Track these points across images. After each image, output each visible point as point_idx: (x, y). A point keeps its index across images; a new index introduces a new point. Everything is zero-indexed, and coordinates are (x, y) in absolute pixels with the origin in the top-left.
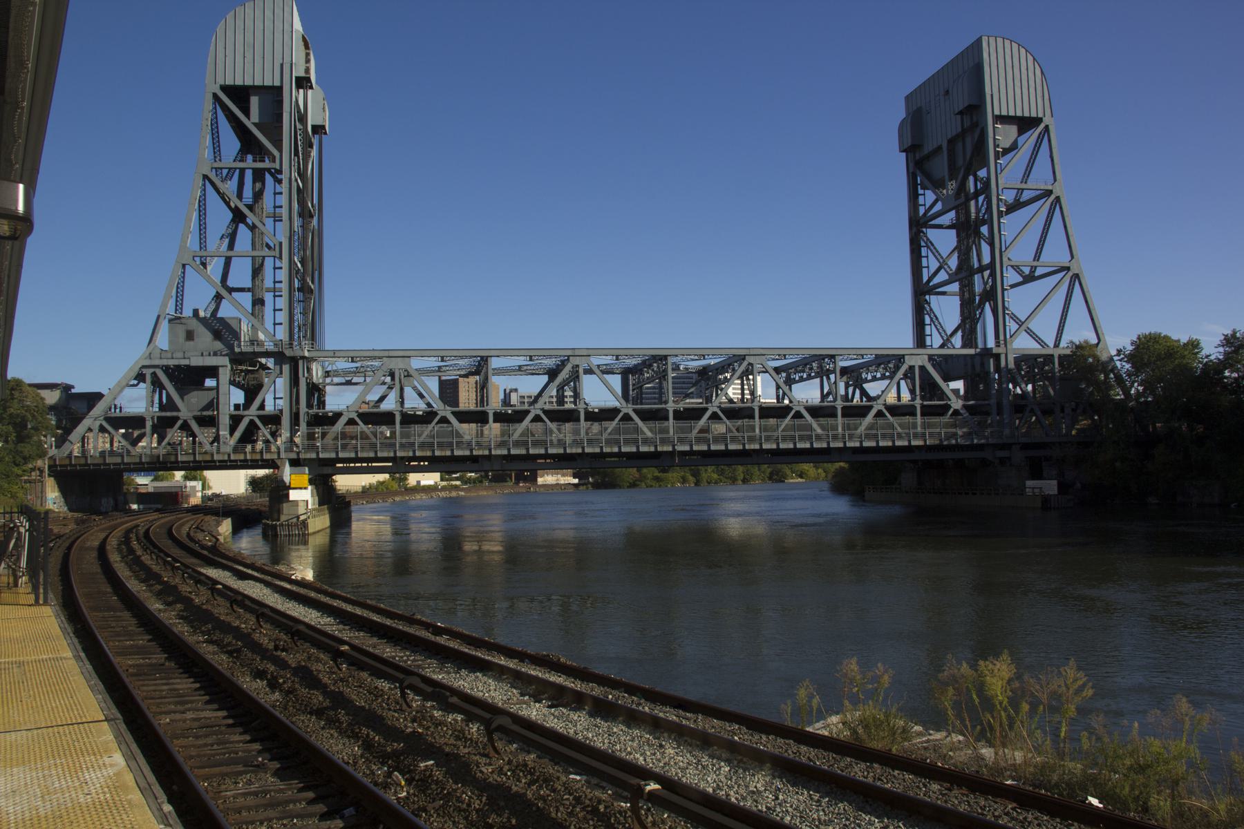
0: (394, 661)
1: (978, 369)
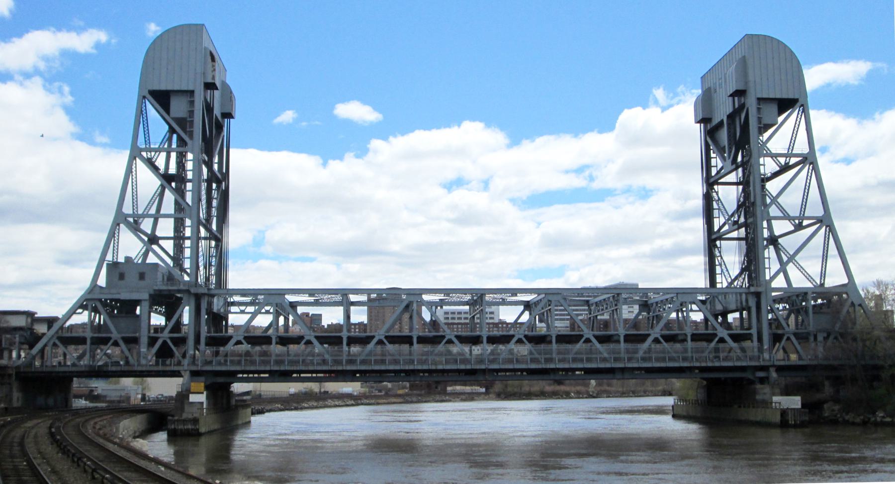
0: (66, 369)
1: (744, 304)
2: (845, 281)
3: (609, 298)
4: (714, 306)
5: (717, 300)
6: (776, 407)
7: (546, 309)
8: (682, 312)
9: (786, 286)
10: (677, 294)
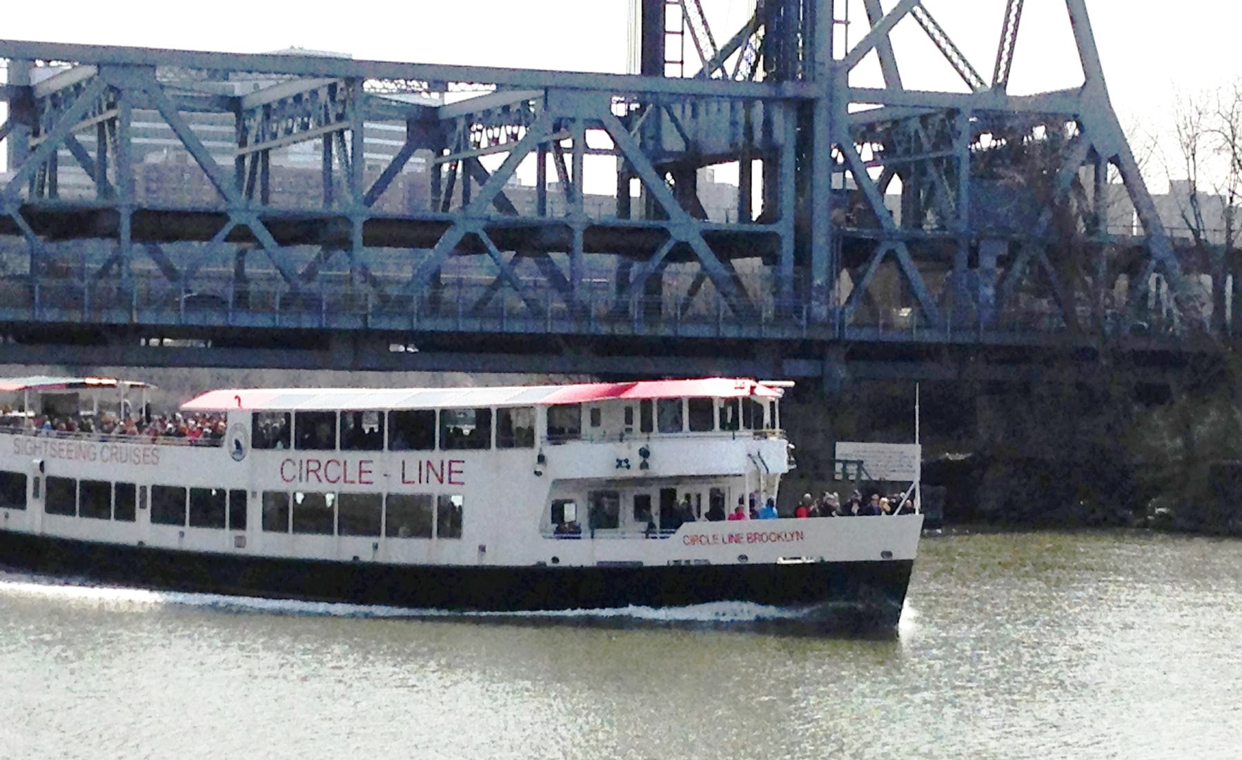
2: (1073, 78)
3: (314, 93)
4: (657, 138)
5: (665, 117)
6: (846, 475)
7: (100, 118)
8: (559, 152)
9: (884, 86)
10: (546, 89)
